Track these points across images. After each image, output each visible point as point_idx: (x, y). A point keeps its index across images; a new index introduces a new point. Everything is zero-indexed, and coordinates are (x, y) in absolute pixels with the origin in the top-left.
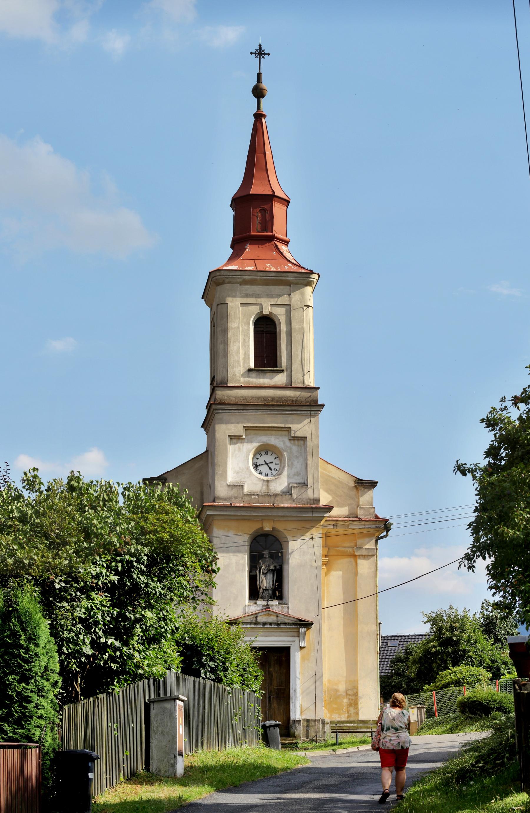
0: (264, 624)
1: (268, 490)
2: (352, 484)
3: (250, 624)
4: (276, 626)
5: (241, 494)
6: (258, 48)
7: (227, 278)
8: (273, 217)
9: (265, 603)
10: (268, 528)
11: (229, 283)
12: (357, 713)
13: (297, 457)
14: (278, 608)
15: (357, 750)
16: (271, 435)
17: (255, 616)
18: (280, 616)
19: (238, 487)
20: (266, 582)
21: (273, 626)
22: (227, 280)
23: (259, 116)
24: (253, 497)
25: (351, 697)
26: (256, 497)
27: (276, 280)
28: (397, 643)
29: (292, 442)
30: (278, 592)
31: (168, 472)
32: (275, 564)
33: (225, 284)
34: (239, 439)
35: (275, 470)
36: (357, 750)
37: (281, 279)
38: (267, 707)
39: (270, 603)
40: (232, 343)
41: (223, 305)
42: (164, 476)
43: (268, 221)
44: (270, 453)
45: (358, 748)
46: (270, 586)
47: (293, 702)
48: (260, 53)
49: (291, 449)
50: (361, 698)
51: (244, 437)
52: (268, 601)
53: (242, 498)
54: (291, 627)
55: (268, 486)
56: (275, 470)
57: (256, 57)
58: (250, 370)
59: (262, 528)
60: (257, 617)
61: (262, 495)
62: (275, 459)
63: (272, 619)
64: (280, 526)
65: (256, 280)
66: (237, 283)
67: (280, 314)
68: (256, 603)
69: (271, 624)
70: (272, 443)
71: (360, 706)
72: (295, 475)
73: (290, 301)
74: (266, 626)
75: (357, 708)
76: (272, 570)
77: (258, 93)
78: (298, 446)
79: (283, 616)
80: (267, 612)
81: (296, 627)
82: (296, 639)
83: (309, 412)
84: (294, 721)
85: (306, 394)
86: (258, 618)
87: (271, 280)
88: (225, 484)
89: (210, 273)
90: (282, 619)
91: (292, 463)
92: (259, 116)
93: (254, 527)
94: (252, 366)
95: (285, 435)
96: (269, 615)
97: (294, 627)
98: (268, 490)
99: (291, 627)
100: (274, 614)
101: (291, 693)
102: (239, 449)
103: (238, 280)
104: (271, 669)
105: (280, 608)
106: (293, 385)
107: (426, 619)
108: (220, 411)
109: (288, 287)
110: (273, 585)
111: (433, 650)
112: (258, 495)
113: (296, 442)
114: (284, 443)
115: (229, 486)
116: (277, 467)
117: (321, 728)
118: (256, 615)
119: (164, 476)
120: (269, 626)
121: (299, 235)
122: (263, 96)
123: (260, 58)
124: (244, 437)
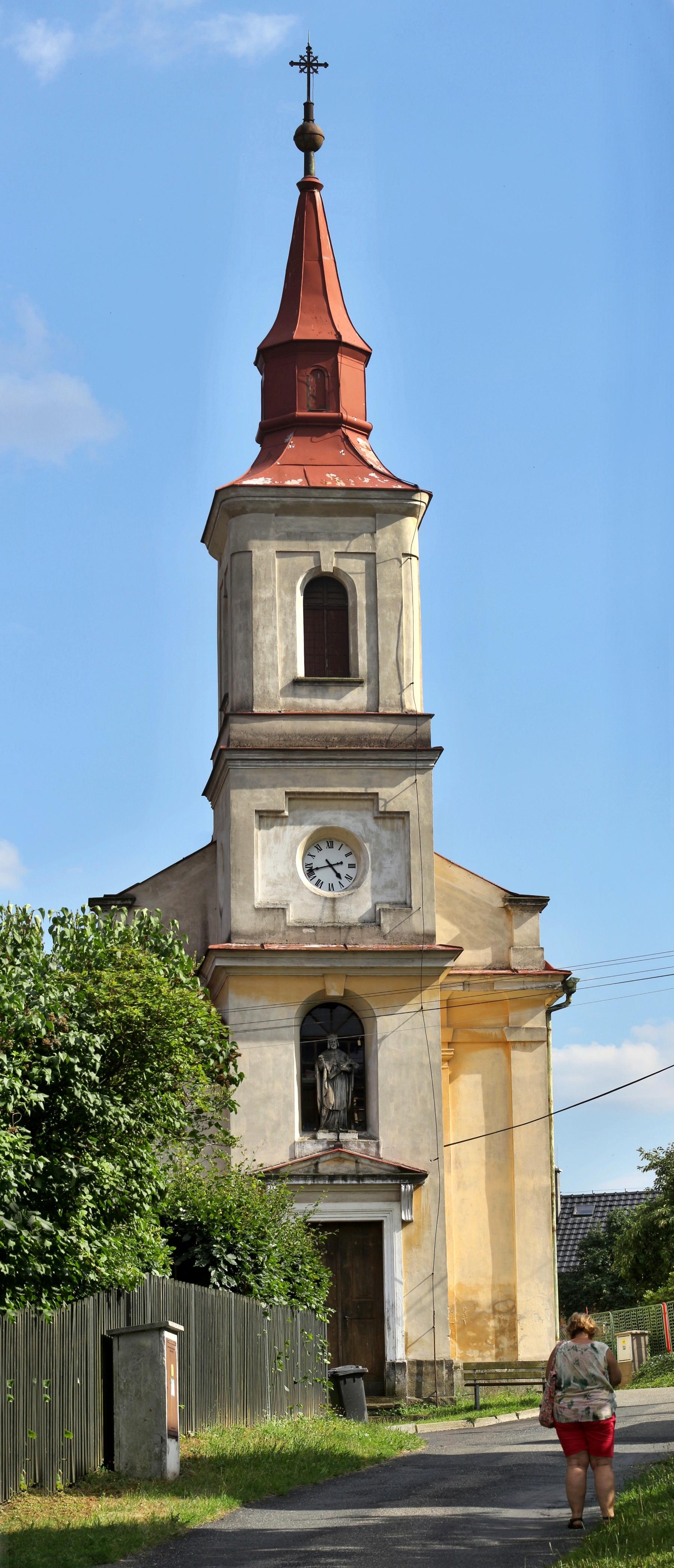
0: (332, 1178)
1: (334, 917)
2: (499, 903)
3: (305, 1177)
4: (355, 1182)
5: (282, 926)
6: (304, 53)
7: (251, 502)
8: (338, 385)
9: (331, 1136)
10: (335, 991)
11: (254, 511)
12: (515, 1348)
13: (390, 852)
14: (359, 1146)
15: (516, 1418)
16: (340, 809)
17: (314, 1162)
18: (363, 1161)
19: (275, 912)
20: (334, 1096)
21: (349, 1182)
22: (250, 507)
23: (308, 187)
24: (305, 930)
25: (503, 1317)
26: (312, 931)
27: (347, 504)
28: (591, 1209)
29: (380, 822)
30: (358, 1114)
31: (138, 884)
32: (349, 1061)
33: (247, 513)
34: (277, 817)
35: (348, 877)
36: (516, 1418)
37: (355, 504)
38: (340, 1339)
39: (344, 1137)
40: (261, 630)
41: (249, 554)
42: (131, 892)
43: (329, 392)
44: (336, 845)
45: (517, 1415)
46: (341, 1104)
47: (389, 1328)
48: (309, 64)
49: (377, 836)
50: (522, 1317)
51: (286, 813)
52: (338, 1133)
53: (284, 934)
54: (385, 1182)
55: (334, 909)
56: (348, 877)
57: (302, 71)
58: (297, 682)
59: (324, 991)
60: (316, 1164)
61: (322, 928)
62: (347, 855)
63: (347, 1167)
64: (358, 987)
65: (306, 505)
66: (269, 511)
67: (354, 570)
68: (315, 1138)
69: (344, 1177)
70: (341, 826)
71: (520, 1333)
72: (386, 887)
73: (375, 548)
74: (335, 1182)
75: (515, 1337)
76: (345, 1072)
77: (307, 140)
78: (392, 830)
79: (367, 1162)
81: (394, 1182)
82: (395, 1206)
83: (413, 764)
84: (393, 1365)
85: (406, 728)
86: (320, 1166)
87: (336, 505)
88: (250, 907)
89: (217, 492)
90: (365, 1167)
91: (381, 864)
92: (308, 187)
93: (307, 990)
94: (301, 673)
95: (367, 809)
96: (341, 1160)
98: (334, 917)
99: (385, 1182)
100: (352, 1158)
101: (386, 1310)
102: (277, 838)
103: (273, 506)
104: (347, 1265)
105: (363, 1146)
106: (381, 710)
107: (647, 1163)
108: (239, 763)
109: (370, 519)
110: (348, 1102)
111: (663, 1222)
112: (314, 927)
113: (388, 822)
114: (365, 824)
115: (257, 910)
116: (352, 872)
117: (446, 1377)
118: (315, 1160)
119: (131, 892)
120: (341, 1182)
121: (392, 420)
122: (316, 148)
123: (309, 73)
124: (286, 813)
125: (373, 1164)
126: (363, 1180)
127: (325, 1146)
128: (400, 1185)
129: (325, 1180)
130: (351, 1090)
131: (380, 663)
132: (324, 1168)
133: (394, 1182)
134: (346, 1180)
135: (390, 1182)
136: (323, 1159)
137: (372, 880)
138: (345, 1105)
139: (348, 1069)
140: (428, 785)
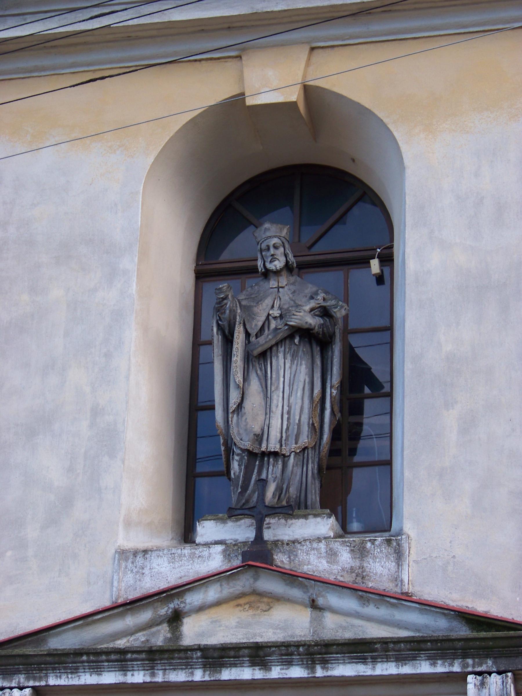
3: (121, 658)
9: (241, 531)
10: (272, 81)
14: (332, 555)
17: (164, 610)
18: (333, 599)
21: (276, 673)
30: (349, 463)
39: (279, 530)
60: (176, 619)
64: (356, 76)
76: (305, 334)
79: (349, 603)
80: (243, 583)
97: (425, 667)
99: (407, 669)
100: (296, 593)
125: (370, 610)
126: (325, 663)
127: (155, 668)
128: (462, 678)
129: (188, 666)
130: (332, 392)
131: (375, 400)
132: (195, 631)
133: (440, 668)
134: (265, 666)
135: (425, 667)
136: (194, 599)
137: (241, 665)
138: (305, 439)
139: (313, 321)
140: (304, 76)
